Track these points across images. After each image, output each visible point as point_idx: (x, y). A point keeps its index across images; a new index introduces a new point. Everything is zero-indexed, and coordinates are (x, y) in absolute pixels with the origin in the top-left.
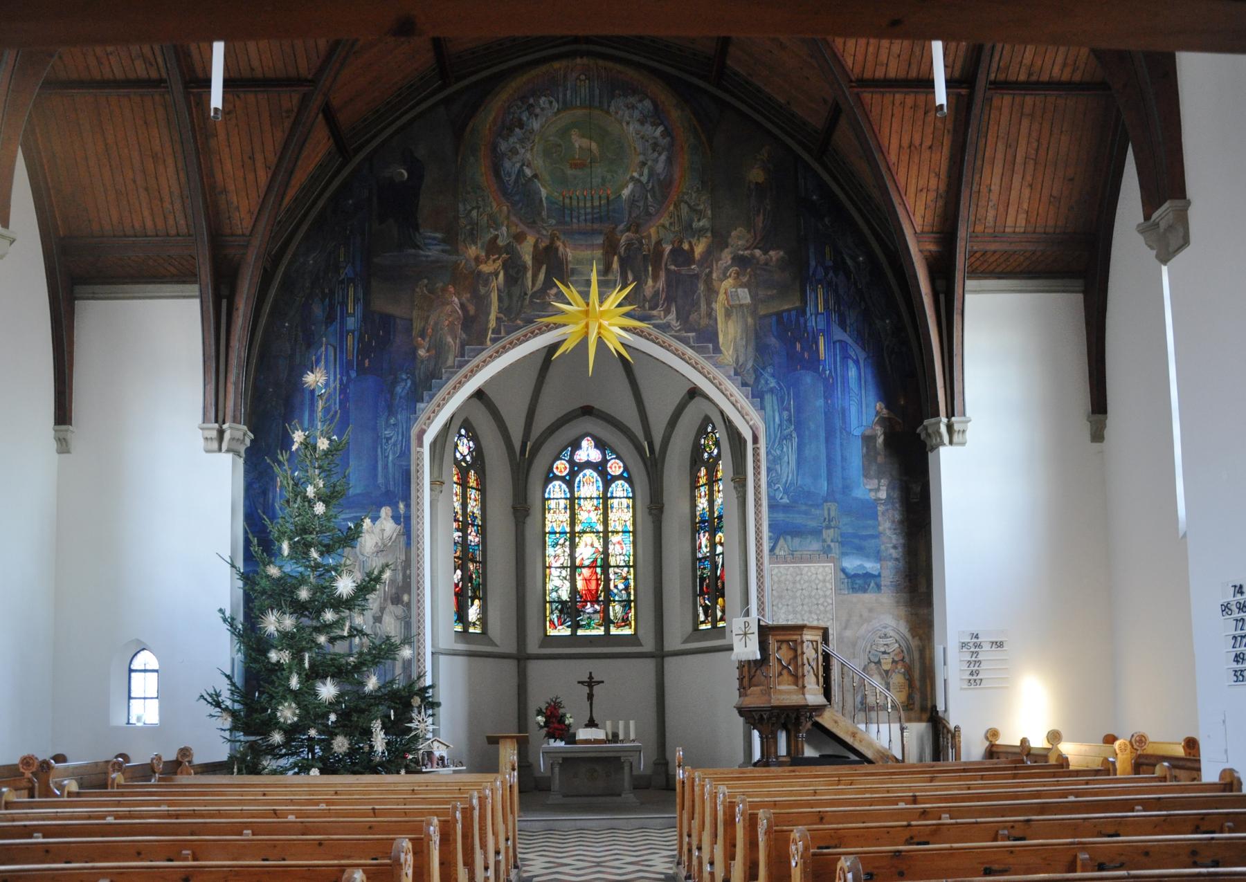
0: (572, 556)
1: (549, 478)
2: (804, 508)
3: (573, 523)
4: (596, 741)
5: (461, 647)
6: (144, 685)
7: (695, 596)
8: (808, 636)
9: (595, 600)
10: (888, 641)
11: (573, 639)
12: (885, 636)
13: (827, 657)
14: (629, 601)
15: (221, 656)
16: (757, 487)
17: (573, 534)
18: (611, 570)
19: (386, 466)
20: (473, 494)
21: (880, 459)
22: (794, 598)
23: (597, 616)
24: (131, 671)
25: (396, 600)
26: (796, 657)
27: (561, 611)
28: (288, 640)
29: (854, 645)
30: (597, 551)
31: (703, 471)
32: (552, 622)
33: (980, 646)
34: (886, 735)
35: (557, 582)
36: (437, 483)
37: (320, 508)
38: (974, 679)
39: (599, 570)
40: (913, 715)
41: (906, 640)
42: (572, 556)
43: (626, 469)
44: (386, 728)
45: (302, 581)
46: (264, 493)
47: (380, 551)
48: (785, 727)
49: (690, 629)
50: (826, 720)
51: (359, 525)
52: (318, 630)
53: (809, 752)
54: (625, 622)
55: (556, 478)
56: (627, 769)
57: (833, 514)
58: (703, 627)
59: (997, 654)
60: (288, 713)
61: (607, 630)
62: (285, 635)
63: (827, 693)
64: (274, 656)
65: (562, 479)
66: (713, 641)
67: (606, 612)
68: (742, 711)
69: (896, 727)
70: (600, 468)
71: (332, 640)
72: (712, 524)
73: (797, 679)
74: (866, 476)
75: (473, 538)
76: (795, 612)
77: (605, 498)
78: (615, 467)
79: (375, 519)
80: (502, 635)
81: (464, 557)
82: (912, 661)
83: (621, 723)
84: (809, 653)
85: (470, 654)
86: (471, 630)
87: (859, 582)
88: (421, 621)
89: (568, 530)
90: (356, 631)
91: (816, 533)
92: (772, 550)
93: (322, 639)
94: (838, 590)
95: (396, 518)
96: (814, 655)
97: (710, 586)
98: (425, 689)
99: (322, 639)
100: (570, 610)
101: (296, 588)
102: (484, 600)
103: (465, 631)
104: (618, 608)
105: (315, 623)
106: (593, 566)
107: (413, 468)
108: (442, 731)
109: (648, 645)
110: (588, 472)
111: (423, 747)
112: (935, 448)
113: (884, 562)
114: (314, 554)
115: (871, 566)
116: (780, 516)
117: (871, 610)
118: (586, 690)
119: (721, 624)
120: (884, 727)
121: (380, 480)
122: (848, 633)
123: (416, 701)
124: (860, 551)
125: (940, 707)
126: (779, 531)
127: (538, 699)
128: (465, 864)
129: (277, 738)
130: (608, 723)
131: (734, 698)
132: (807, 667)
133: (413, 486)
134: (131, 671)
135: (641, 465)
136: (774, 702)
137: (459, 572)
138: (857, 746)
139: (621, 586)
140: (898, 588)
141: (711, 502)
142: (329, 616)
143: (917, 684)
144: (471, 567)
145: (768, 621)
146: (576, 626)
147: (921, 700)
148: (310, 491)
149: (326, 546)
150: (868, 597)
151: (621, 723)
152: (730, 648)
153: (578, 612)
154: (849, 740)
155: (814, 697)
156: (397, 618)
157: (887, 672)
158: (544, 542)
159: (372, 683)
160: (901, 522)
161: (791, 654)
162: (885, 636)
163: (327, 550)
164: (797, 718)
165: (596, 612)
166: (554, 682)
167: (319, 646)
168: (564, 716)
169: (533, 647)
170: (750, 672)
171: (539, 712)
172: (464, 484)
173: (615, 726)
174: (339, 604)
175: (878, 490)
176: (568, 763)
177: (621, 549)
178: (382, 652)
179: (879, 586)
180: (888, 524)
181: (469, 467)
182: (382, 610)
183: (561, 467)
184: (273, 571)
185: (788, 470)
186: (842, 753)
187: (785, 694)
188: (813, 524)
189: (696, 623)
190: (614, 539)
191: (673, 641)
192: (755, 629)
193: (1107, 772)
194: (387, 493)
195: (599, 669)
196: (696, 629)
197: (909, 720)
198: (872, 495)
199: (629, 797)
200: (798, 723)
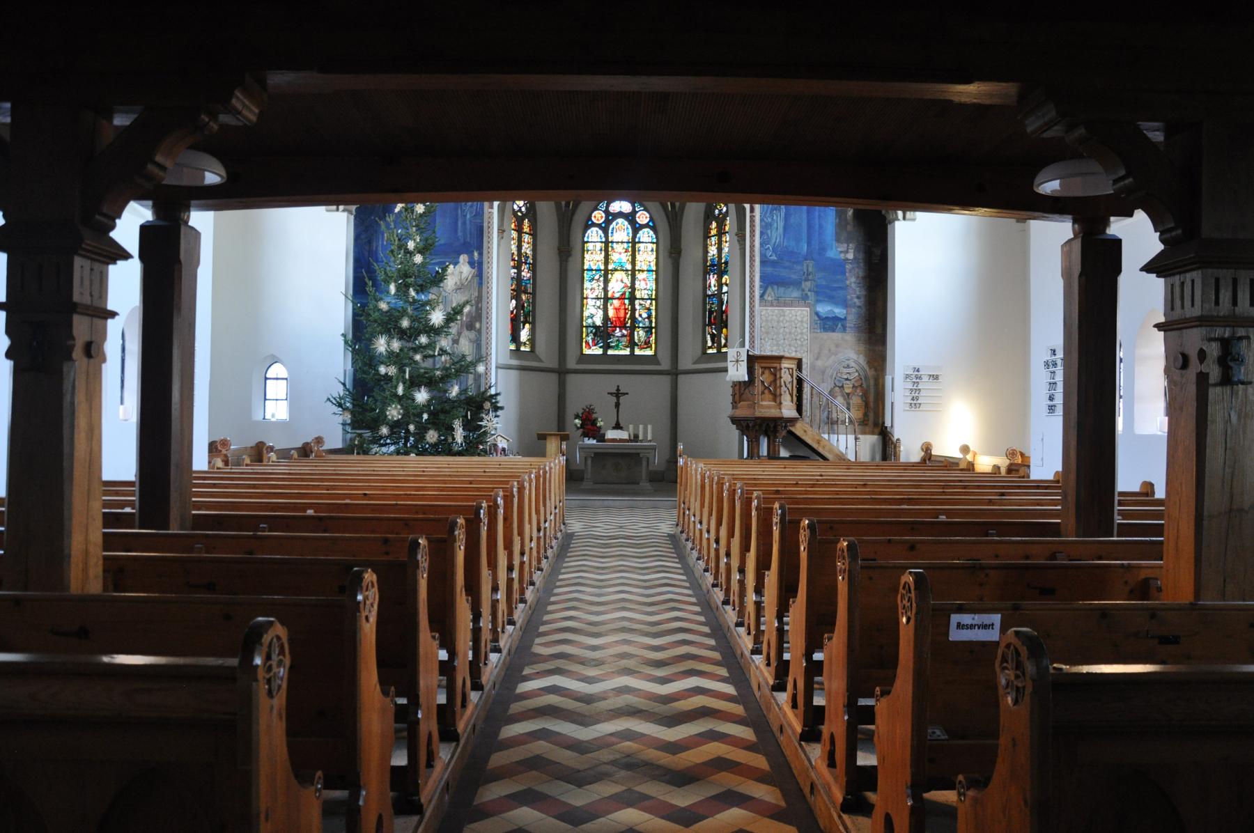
0: (605, 290)
1: (588, 225)
2: (787, 264)
3: (606, 262)
4: (621, 440)
5: (515, 362)
6: (277, 390)
7: (705, 325)
8: (785, 364)
9: (623, 326)
10: (850, 370)
11: (604, 358)
12: (848, 367)
13: (800, 382)
14: (651, 328)
15: (335, 365)
16: (752, 246)
17: (606, 271)
18: (637, 302)
19: (464, 223)
20: (526, 238)
21: (850, 228)
22: (778, 334)
23: (625, 339)
24: (266, 379)
25: (470, 327)
26: (775, 380)
27: (595, 335)
28: (392, 358)
29: (823, 373)
30: (626, 286)
31: (714, 225)
32: (587, 343)
33: (920, 378)
34: (849, 445)
35: (593, 311)
36: (501, 231)
37: (418, 259)
38: (915, 403)
39: (627, 302)
40: (867, 429)
41: (863, 368)
42: (605, 290)
43: (651, 219)
44: (466, 426)
45: (403, 313)
46: (370, 242)
47: (460, 288)
48: (766, 434)
49: (700, 353)
50: (798, 429)
51: (444, 270)
52: (416, 350)
53: (784, 453)
54: (647, 344)
55: (594, 225)
56: (644, 464)
57: (810, 269)
58: (710, 351)
59: (934, 385)
60: (394, 413)
61: (632, 351)
62: (391, 354)
63: (799, 409)
64: (382, 370)
65: (599, 226)
66: (715, 364)
67: (631, 335)
68: (735, 420)
69: (851, 438)
70: (630, 218)
71: (425, 357)
72: (720, 268)
73: (776, 397)
74: (838, 240)
75: (526, 274)
76: (778, 345)
77: (634, 243)
78: (643, 218)
79: (456, 264)
80: (547, 355)
81: (519, 289)
82: (868, 387)
83: (641, 427)
84: (786, 377)
85: (522, 369)
86: (522, 349)
87: (828, 324)
88: (488, 344)
89: (602, 267)
90: (443, 352)
91: (797, 284)
92: (762, 296)
93: (418, 357)
94: (812, 329)
95: (471, 264)
96: (790, 379)
97: (717, 319)
98: (492, 396)
99: (418, 357)
100: (603, 334)
101: (400, 318)
102: (533, 324)
103: (518, 349)
104: (642, 333)
105: (410, 345)
106: (622, 298)
107: (485, 225)
108: (501, 427)
109: (665, 365)
110: (620, 220)
111: (490, 440)
112: (892, 222)
113: (849, 310)
114: (412, 293)
115: (839, 311)
116: (769, 270)
117: (837, 346)
118: (615, 399)
119: (724, 350)
120: (842, 437)
121: (460, 234)
122: (819, 363)
123: (487, 405)
124: (831, 299)
125: (888, 424)
126: (767, 281)
127: (575, 405)
128: (505, 548)
129: (384, 430)
130: (631, 427)
131: (727, 410)
132: (784, 388)
133: (485, 239)
134: (266, 379)
135: (665, 219)
136: (758, 414)
137: (514, 302)
138: (820, 450)
139: (645, 315)
140: (858, 329)
141: (720, 250)
142: (423, 340)
143: (872, 404)
144: (524, 297)
145: (757, 352)
146: (607, 347)
147: (873, 417)
148: (411, 245)
149: (421, 286)
150: (836, 336)
151: (641, 427)
152: (725, 370)
153: (609, 336)
154: (815, 446)
155: (788, 411)
156: (471, 341)
157: (848, 394)
158: (583, 278)
159: (455, 391)
160: (864, 278)
161: (771, 378)
162: (848, 367)
163: (421, 289)
164: (775, 427)
165: (623, 336)
166: (587, 392)
167: (416, 362)
168: (596, 419)
169: (571, 364)
170: (741, 390)
171: (577, 416)
172: (520, 230)
173: (636, 428)
174: (434, 331)
175: (847, 252)
176: (599, 457)
177: (646, 285)
178: (461, 367)
179: (844, 328)
180: (853, 280)
181: (524, 216)
182: (459, 334)
183: (598, 216)
184: (383, 306)
185: (776, 234)
186: (805, 451)
187: (766, 409)
188: (794, 277)
189: (705, 347)
190: (640, 276)
191: (686, 362)
192: (745, 358)
193: (1147, 494)
194: (465, 243)
195: (625, 382)
196: (704, 353)
197: (864, 433)
198: (842, 256)
199: (645, 485)
200: (775, 431)
